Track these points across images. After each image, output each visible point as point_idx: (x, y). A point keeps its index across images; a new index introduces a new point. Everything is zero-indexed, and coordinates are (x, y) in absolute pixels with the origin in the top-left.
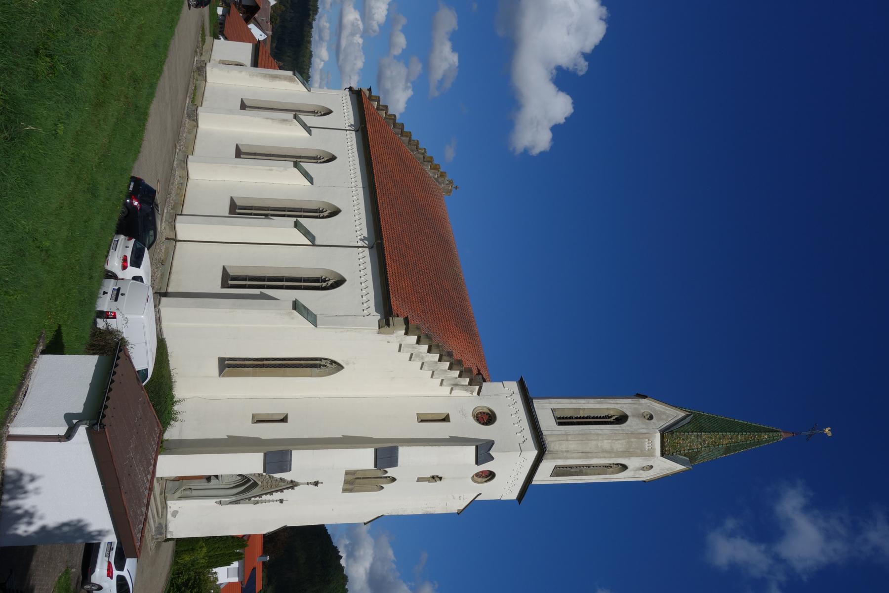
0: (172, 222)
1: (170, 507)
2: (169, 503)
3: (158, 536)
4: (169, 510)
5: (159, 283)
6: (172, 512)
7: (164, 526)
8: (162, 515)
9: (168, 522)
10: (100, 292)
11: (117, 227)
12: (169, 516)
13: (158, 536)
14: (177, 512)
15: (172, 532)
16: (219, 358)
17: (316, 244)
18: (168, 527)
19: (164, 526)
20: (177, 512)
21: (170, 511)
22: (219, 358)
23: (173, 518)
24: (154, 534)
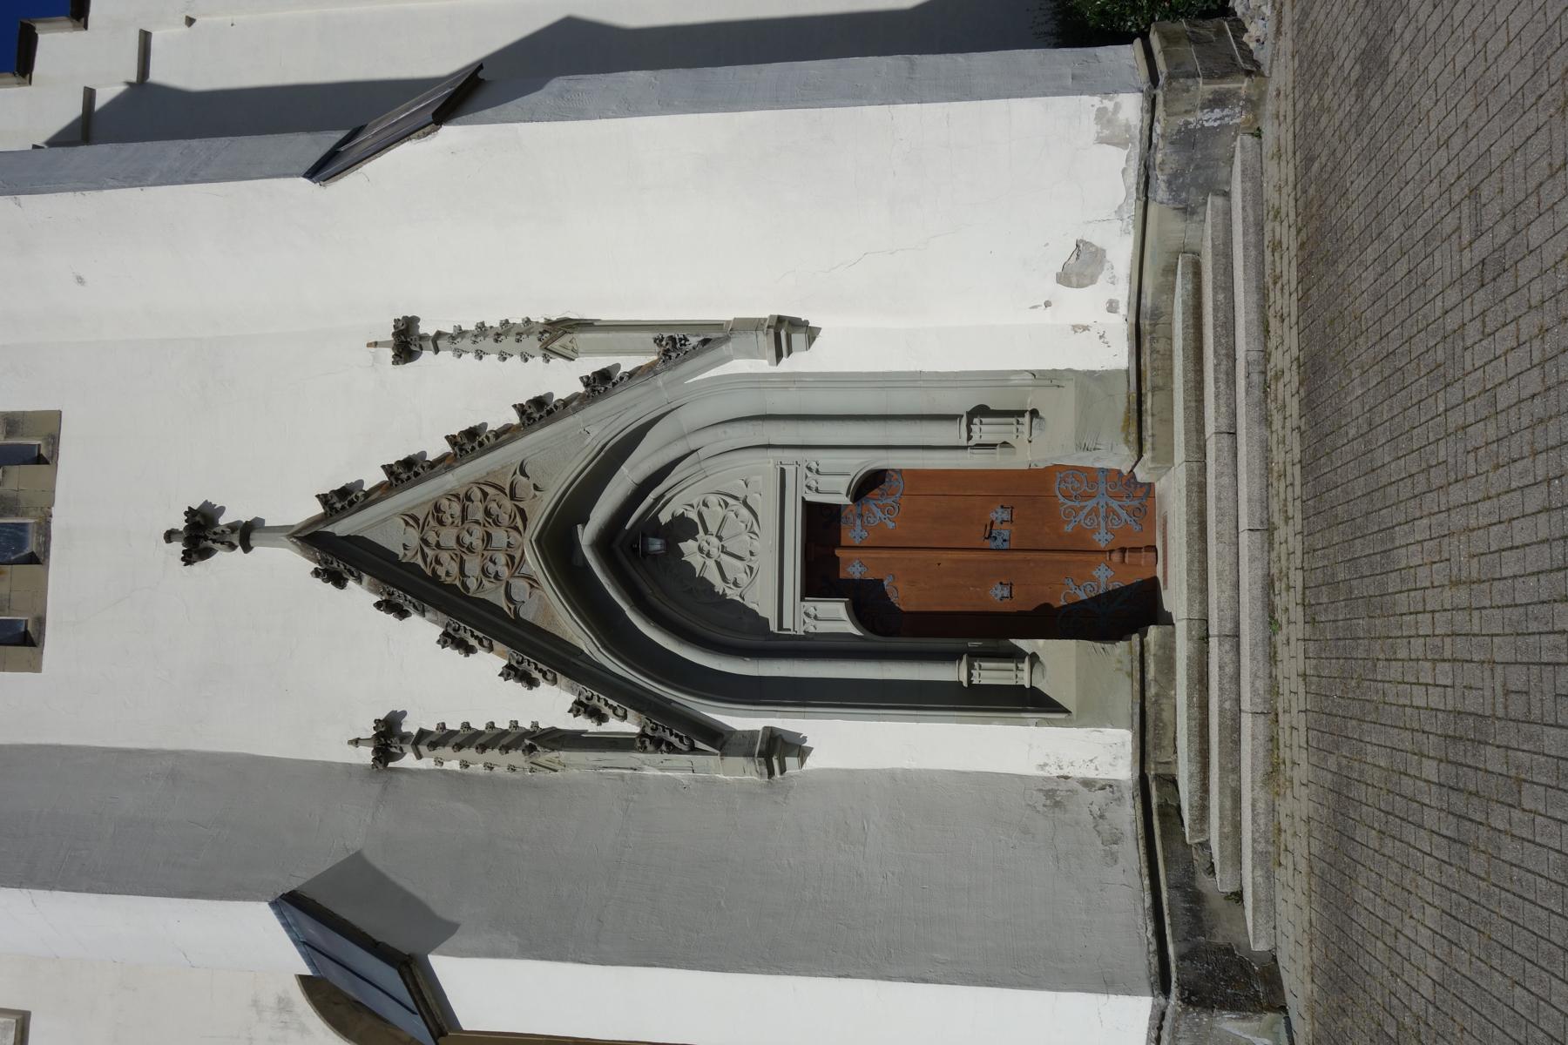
0: (1392, 743)
1: (1112, 307)
2: (1115, 356)
3: (1211, 118)
4: (1122, 292)
5: (1268, 922)
6: (1103, 279)
7: (1161, 191)
8: (1170, 270)
9: (1132, 209)
10: (450, 741)
11: (915, 770)
12: (1121, 253)
13: (1211, 118)
14: (1064, 278)
15: (1102, 140)
16: (85, 88)
17: (439, 1041)
18: (1132, 177)
19: (1161, 191)
20: (1064, 278)
21: (1115, 284)
22: (85, 88)
23: (1096, 239)
24: (1242, 146)
